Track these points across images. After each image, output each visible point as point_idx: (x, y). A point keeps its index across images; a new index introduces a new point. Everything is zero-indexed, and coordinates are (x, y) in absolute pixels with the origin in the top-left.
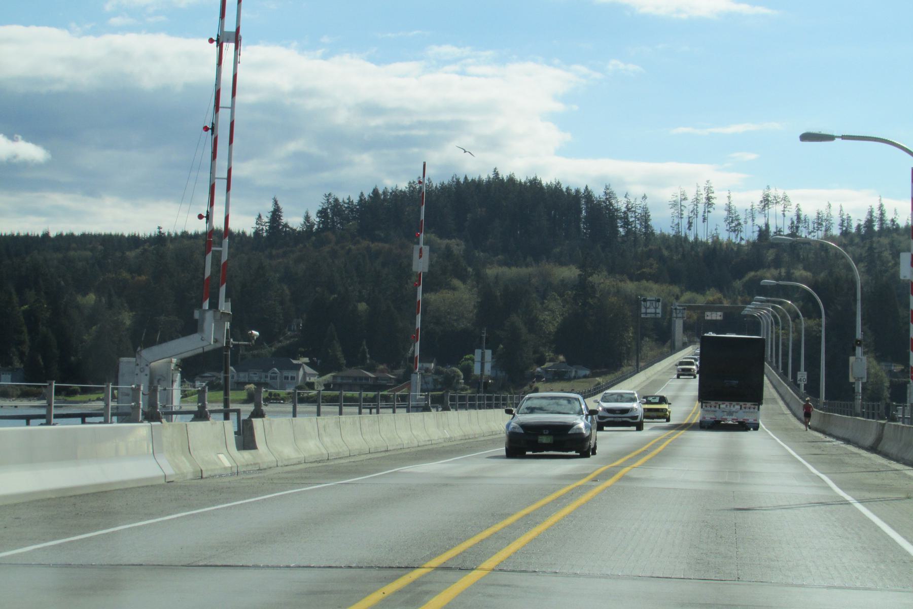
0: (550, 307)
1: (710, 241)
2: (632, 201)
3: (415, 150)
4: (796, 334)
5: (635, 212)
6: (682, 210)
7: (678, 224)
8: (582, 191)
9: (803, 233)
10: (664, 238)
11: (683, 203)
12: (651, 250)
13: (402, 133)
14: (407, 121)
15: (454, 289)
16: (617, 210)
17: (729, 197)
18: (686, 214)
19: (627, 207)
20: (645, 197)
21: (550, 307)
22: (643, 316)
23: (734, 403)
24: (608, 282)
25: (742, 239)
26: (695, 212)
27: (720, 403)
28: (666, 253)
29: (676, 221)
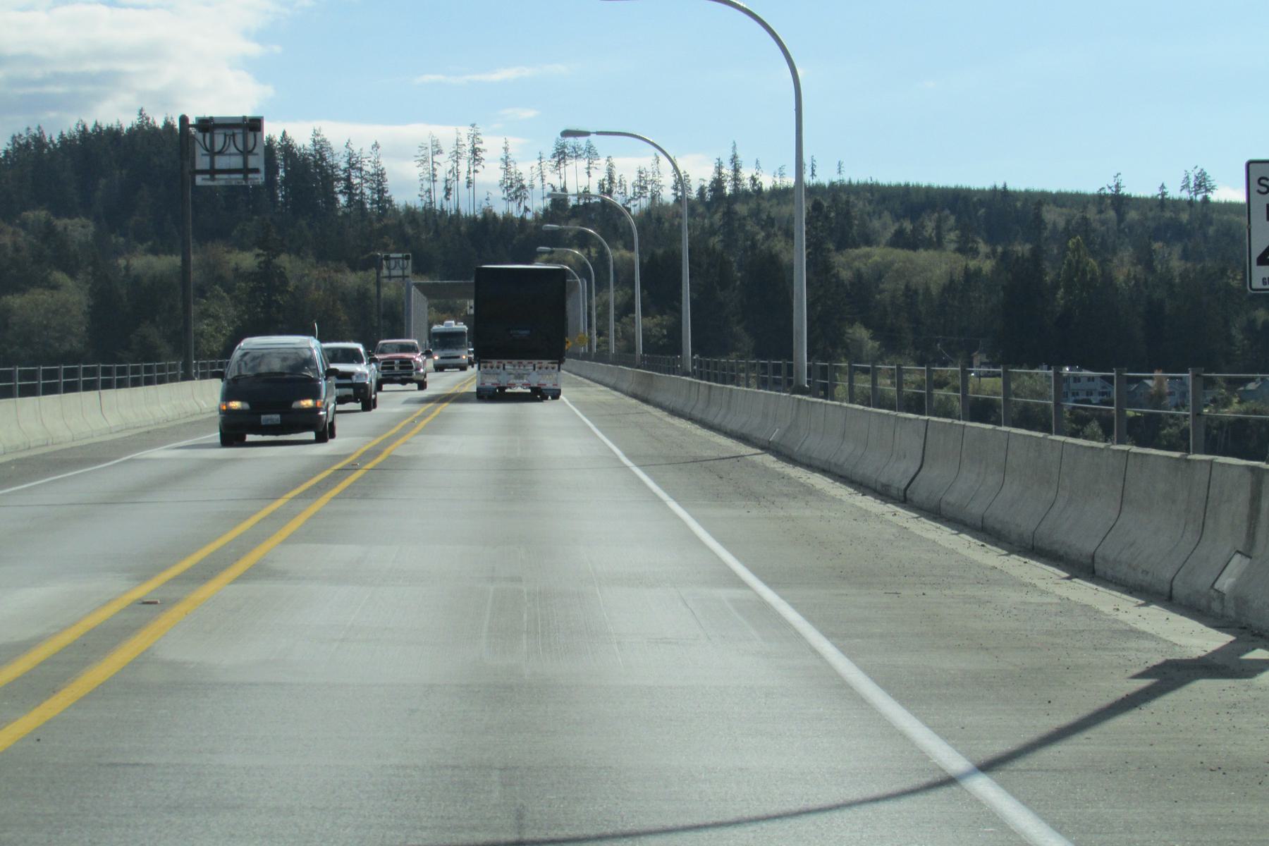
0: (212, 310)
1: (480, 216)
2: (357, 151)
3: (53, 115)
4: (622, 343)
5: (361, 169)
6: (434, 169)
7: (429, 191)
8: (278, 138)
9: (618, 199)
10: (410, 213)
11: (436, 158)
12: (386, 226)
13: (32, 90)
14: (37, 73)
15: (55, 287)
16: (333, 167)
17: (506, 149)
18: (442, 173)
19: (349, 162)
20: (376, 146)
21: (212, 310)
22: (199, 180)
23: (525, 362)
24: (315, 272)
25: (526, 209)
26: (455, 173)
27: (505, 361)
28: (409, 230)
29: (427, 185)
